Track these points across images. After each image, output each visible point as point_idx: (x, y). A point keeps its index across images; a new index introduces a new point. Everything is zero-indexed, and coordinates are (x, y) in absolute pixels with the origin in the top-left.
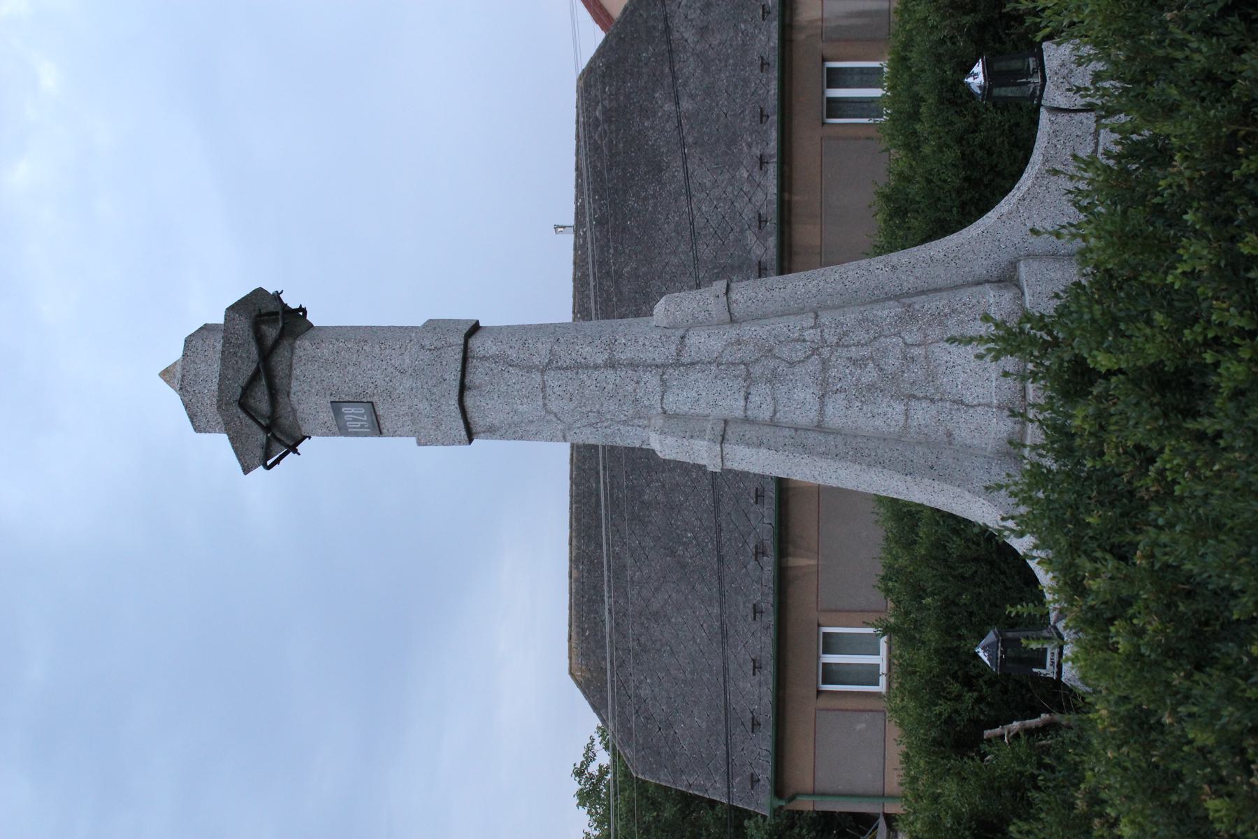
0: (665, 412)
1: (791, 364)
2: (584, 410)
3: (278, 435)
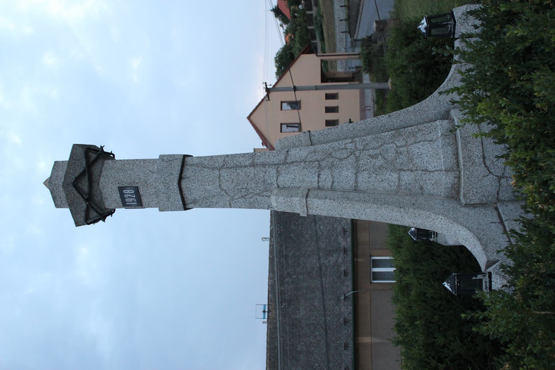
0: (278, 187)
1: (341, 160)
2: (239, 187)
3: (93, 205)
